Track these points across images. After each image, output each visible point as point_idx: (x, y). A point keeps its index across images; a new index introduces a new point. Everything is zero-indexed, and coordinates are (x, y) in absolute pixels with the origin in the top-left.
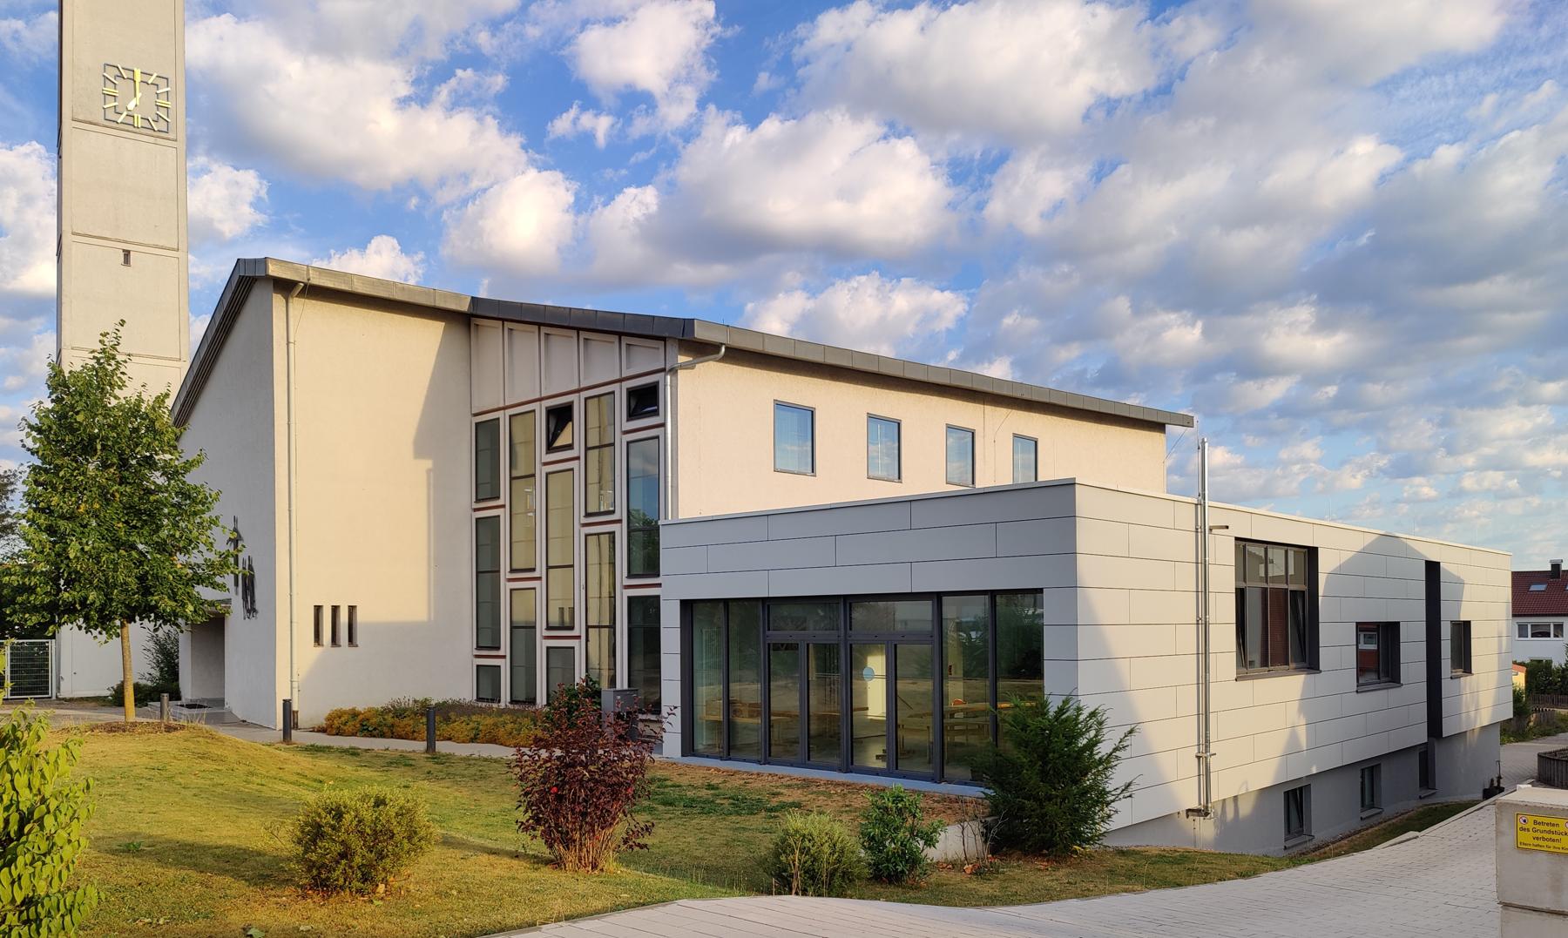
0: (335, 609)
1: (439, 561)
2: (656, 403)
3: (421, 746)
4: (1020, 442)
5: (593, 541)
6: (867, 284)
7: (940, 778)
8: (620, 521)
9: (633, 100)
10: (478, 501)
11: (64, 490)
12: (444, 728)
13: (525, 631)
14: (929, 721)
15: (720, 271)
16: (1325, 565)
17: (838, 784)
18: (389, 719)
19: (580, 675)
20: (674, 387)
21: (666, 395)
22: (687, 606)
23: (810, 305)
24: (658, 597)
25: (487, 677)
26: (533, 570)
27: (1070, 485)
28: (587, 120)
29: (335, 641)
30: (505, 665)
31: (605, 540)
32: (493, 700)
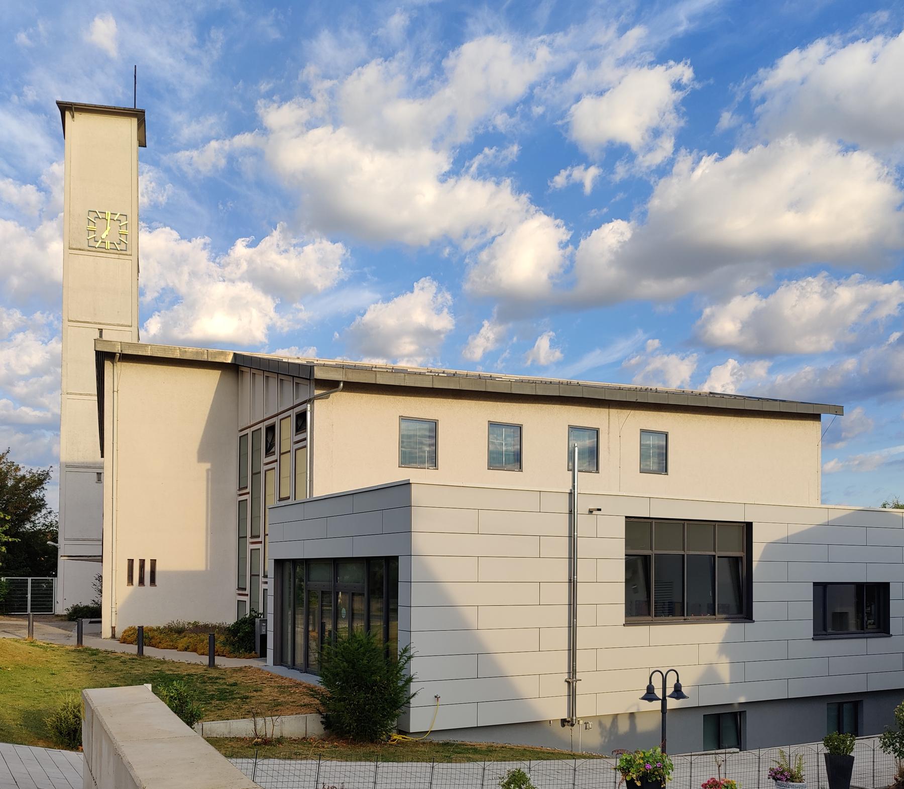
0: (142, 562)
1: (214, 529)
3: (205, 660)
6: (814, 284)
9: (616, 152)
15: (680, 284)
23: (763, 304)
27: (407, 484)
28: (577, 173)
29: (141, 582)
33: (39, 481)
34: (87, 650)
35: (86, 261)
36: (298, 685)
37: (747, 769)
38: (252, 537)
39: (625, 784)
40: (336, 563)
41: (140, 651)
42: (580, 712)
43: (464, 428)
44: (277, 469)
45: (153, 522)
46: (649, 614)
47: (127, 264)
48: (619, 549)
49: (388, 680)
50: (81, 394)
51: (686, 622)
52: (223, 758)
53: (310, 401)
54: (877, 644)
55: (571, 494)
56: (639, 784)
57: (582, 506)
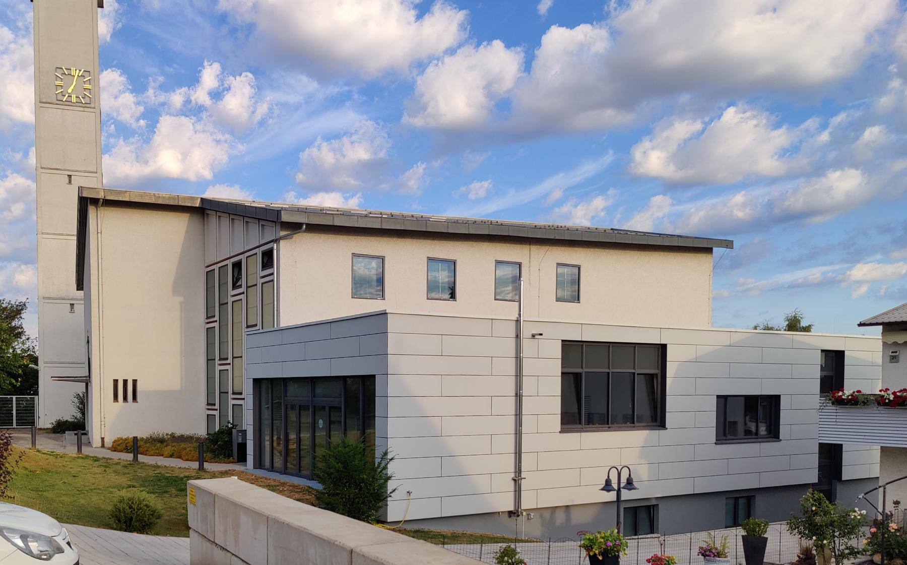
0: (125, 382)
3: (196, 465)
13: (223, 393)
16: (671, 355)
26: (227, 359)
29: (125, 399)
33: (17, 311)
34: (87, 457)
35: (54, 113)
36: (283, 484)
37: (682, 548)
38: (220, 359)
39: (588, 558)
40: (313, 381)
41: (135, 458)
42: (525, 505)
43: (406, 263)
44: (244, 302)
45: (136, 350)
46: (580, 423)
47: (89, 117)
48: (556, 368)
49: (373, 478)
50: (62, 235)
51: (610, 429)
53: (276, 241)
54: (769, 447)
55: (518, 321)
56: (600, 558)
57: (526, 332)
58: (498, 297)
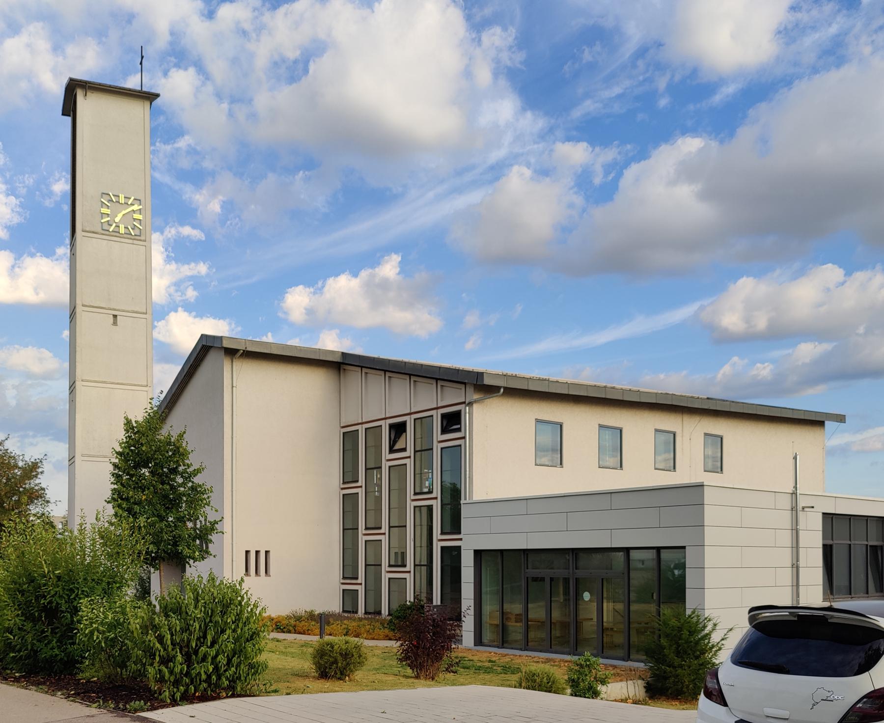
0: (257, 552)
2: (459, 423)
4: (710, 439)
5: (417, 509)
7: (627, 658)
8: (436, 498)
10: (344, 483)
11: (134, 488)
12: (328, 629)
13: (374, 566)
14: (622, 626)
17: (567, 661)
18: (292, 622)
19: (410, 597)
20: (471, 414)
21: (466, 418)
22: (478, 554)
24: (460, 547)
25: (349, 596)
26: (380, 528)
27: (701, 486)
30: (361, 590)
31: (424, 510)
32: (353, 612)
52: (591, 700)
55: (794, 494)
58: (538, 463)
